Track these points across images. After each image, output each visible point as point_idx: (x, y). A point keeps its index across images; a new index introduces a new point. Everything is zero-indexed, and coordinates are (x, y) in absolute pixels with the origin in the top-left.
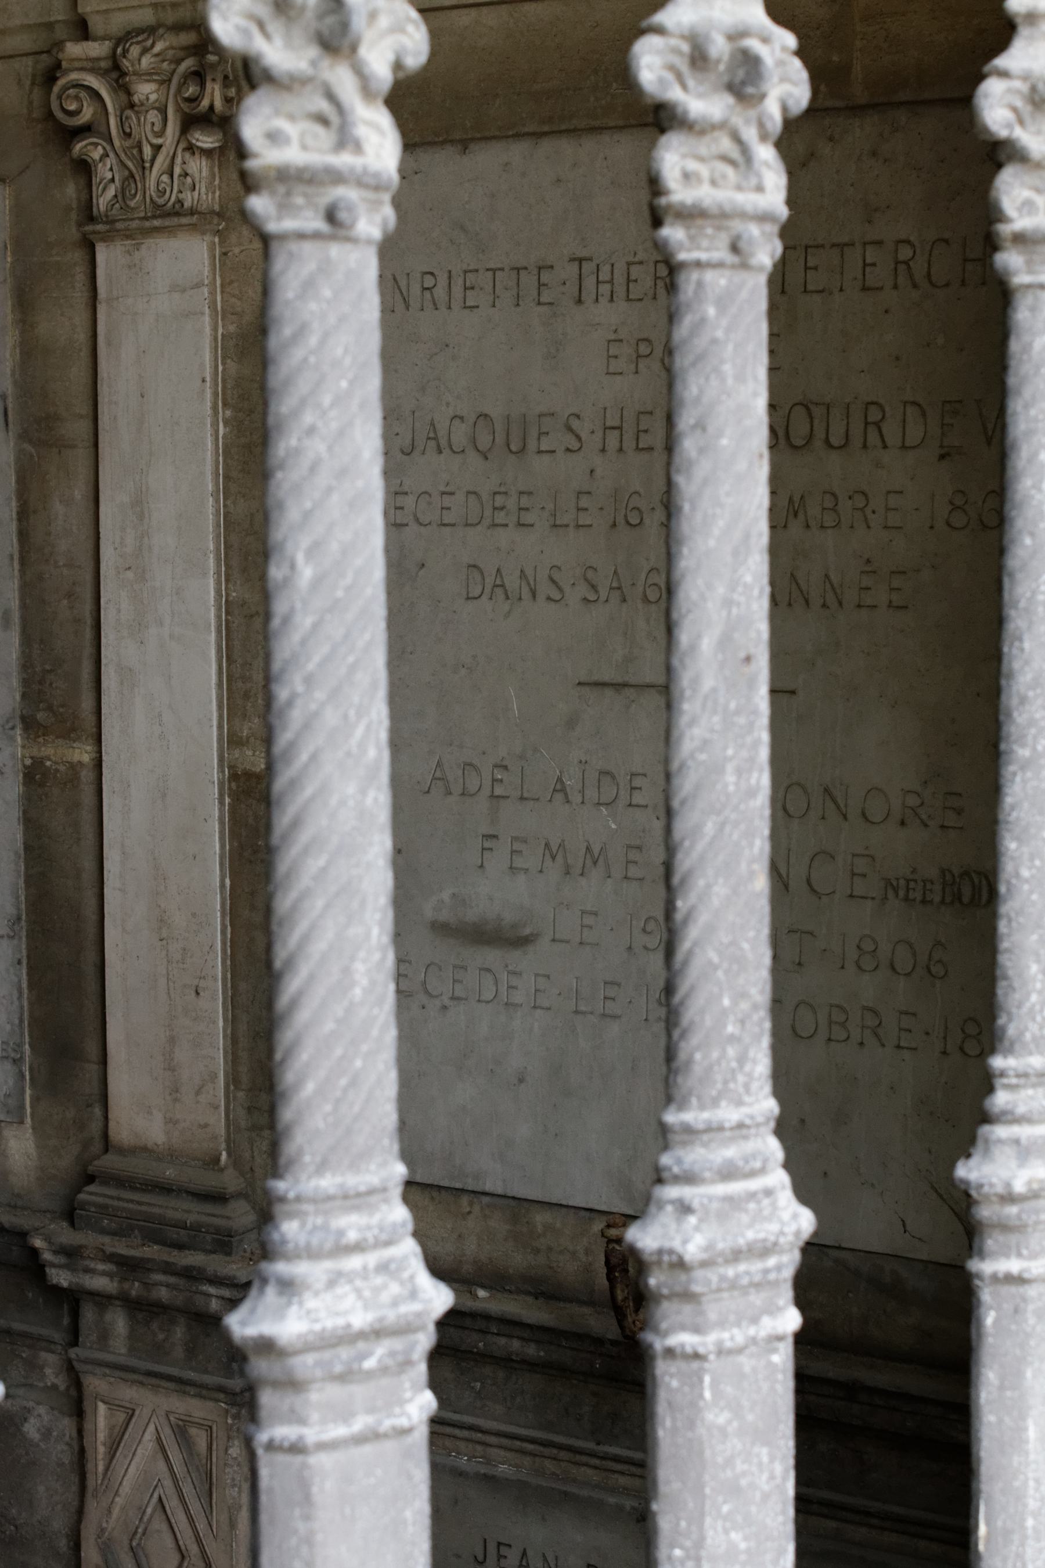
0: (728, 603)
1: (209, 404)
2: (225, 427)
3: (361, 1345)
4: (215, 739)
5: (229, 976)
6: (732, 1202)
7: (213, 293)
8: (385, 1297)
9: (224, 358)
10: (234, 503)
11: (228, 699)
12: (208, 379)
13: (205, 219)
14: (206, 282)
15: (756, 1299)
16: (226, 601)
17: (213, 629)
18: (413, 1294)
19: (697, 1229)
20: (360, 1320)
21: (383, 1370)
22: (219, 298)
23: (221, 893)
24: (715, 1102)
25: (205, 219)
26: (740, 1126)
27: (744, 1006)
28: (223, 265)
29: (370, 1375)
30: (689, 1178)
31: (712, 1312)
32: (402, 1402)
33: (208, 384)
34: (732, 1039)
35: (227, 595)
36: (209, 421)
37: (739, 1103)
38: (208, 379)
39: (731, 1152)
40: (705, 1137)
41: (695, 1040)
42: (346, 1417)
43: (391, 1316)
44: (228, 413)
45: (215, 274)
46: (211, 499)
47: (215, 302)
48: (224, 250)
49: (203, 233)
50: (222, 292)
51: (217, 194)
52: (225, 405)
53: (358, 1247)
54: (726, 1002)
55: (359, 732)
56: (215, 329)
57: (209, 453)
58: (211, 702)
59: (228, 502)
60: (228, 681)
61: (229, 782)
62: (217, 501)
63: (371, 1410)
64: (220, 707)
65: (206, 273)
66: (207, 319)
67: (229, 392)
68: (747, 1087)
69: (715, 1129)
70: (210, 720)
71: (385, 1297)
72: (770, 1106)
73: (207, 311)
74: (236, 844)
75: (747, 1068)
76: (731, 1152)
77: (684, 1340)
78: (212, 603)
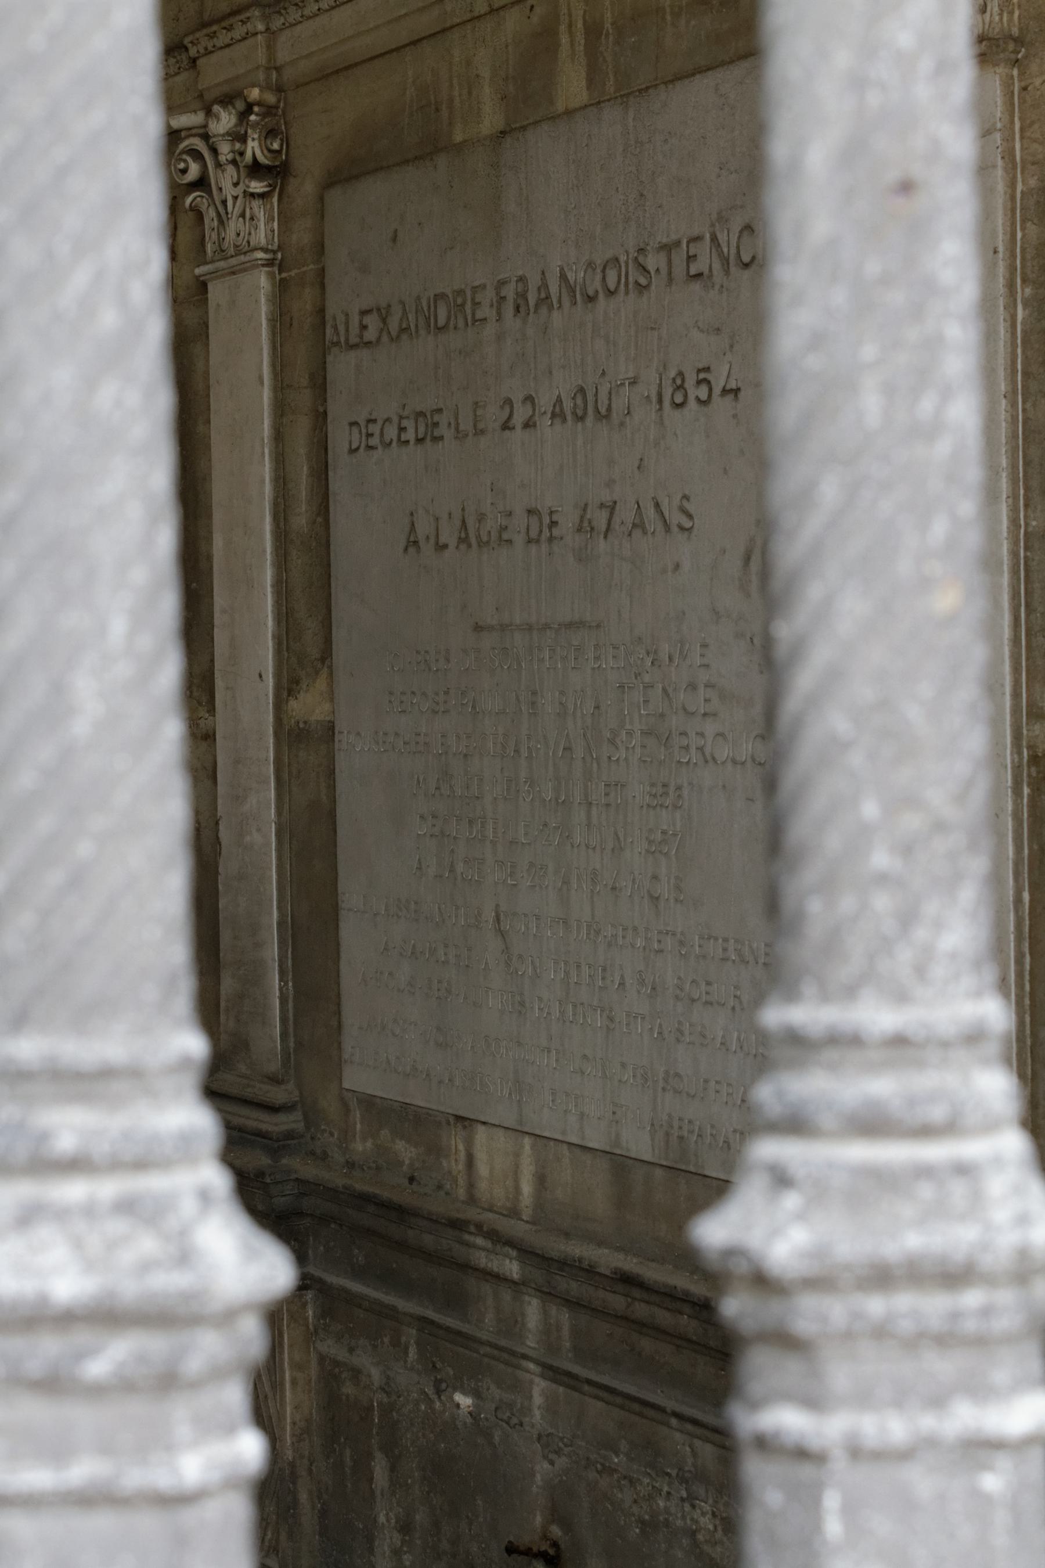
0: (858, 83)
1: (1001, 280)
2: (1024, 309)
3: (81, 1337)
4: (1008, 710)
5: (1028, 1019)
6: (884, 1181)
7: (1009, 139)
8: (128, 1257)
9: (1023, 221)
10: (1034, 405)
11: (1027, 659)
12: (1001, 249)
13: (998, 46)
14: (999, 125)
15: (942, 1366)
16: (1026, 533)
17: (1005, 568)
18: (184, 1256)
19: (801, 1216)
20: (68, 1286)
21: (124, 1385)
22: (1018, 146)
23: (1016, 910)
24: (850, 992)
25: (998, 46)
26: (899, 1041)
27: (912, 822)
28: (1023, 101)
29: (96, 1391)
30: (796, 1124)
31: (840, 1375)
32: (170, 1448)
33: (1001, 255)
34: (882, 879)
35: (1027, 524)
36: (1001, 302)
37: (901, 997)
38: (1001, 249)
39: (882, 1087)
40: (831, 1054)
41: (809, 875)
42: (59, 1453)
43: (130, 1290)
44: (1028, 291)
45: (1012, 116)
46: (1004, 402)
47: (1011, 152)
48: (1023, 84)
49: (996, 65)
50: (1022, 138)
51: (1017, 13)
52: (1024, 281)
53: (76, 1165)
54: (870, 809)
55: (80, 279)
56: (1013, 185)
57: (1002, 343)
58: (1003, 661)
59: (1028, 405)
60: (1027, 635)
61: (1029, 767)
62: (1014, 404)
63: (106, 1448)
64: (1016, 669)
65: (999, 115)
66: (1000, 172)
67: (1029, 264)
68: (920, 971)
69: (845, 1042)
70: (1003, 685)
71: (128, 1257)
72: (995, 1013)
73: (1000, 163)
74: (1036, 847)
75: (921, 933)
76: (882, 1087)
77: (786, 1420)
78: (1005, 534)
